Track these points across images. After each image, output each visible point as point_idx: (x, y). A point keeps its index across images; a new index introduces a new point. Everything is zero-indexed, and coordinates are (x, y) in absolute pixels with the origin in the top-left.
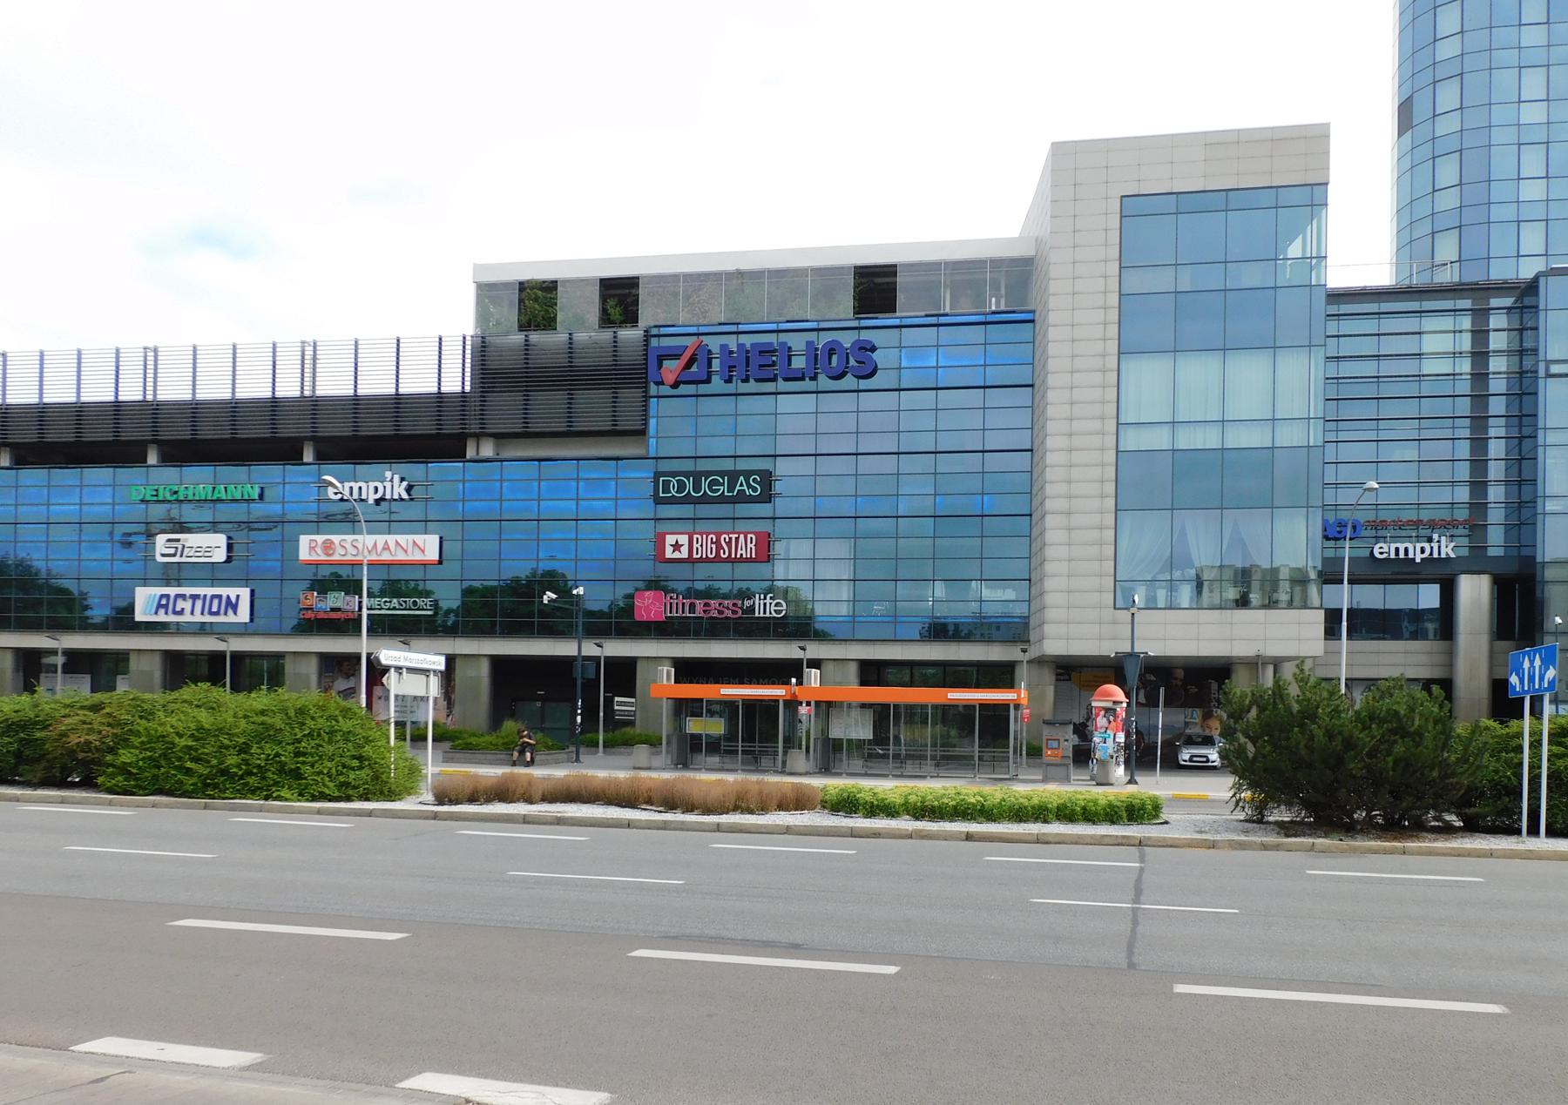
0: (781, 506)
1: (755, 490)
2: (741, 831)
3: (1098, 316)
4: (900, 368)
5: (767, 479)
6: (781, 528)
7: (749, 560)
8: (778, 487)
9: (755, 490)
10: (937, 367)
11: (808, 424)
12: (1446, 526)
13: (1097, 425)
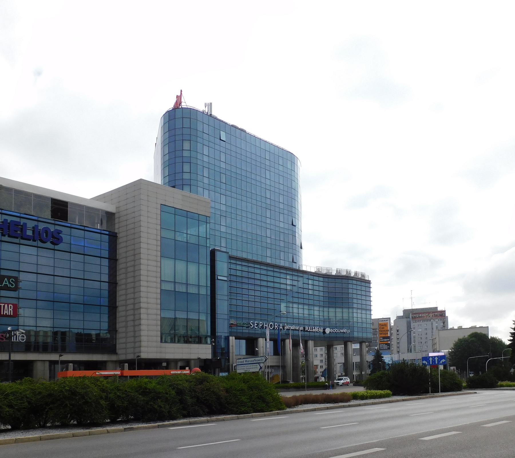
0: (22, 294)
1: (12, 285)
2: (51, 439)
3: (155, 242)
4: (84, 246)
5: (17, 280)
6: (22, 303)
7: (10, 316)
8: (21, 285)
9: (12, 285)
10: (84, 246)
11: (34, 260)
12: (87, 306)
13: (154, 279)
